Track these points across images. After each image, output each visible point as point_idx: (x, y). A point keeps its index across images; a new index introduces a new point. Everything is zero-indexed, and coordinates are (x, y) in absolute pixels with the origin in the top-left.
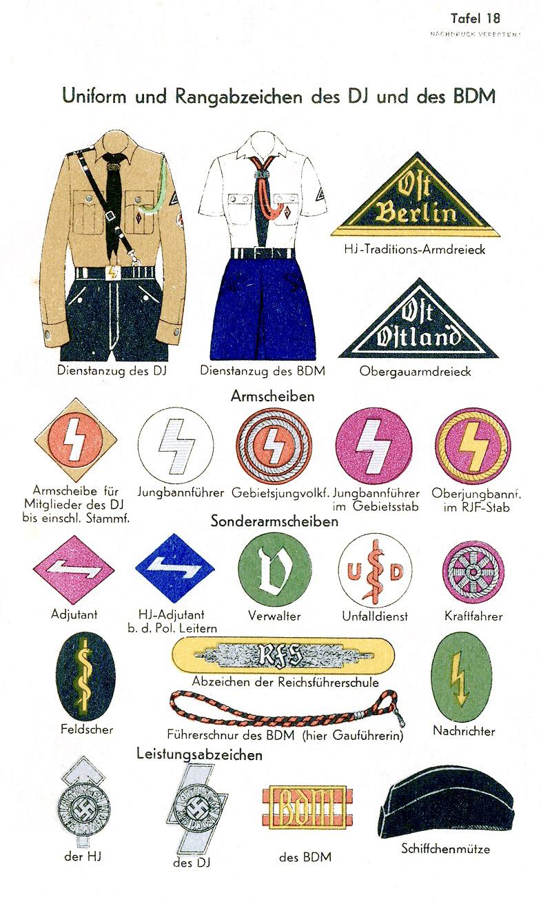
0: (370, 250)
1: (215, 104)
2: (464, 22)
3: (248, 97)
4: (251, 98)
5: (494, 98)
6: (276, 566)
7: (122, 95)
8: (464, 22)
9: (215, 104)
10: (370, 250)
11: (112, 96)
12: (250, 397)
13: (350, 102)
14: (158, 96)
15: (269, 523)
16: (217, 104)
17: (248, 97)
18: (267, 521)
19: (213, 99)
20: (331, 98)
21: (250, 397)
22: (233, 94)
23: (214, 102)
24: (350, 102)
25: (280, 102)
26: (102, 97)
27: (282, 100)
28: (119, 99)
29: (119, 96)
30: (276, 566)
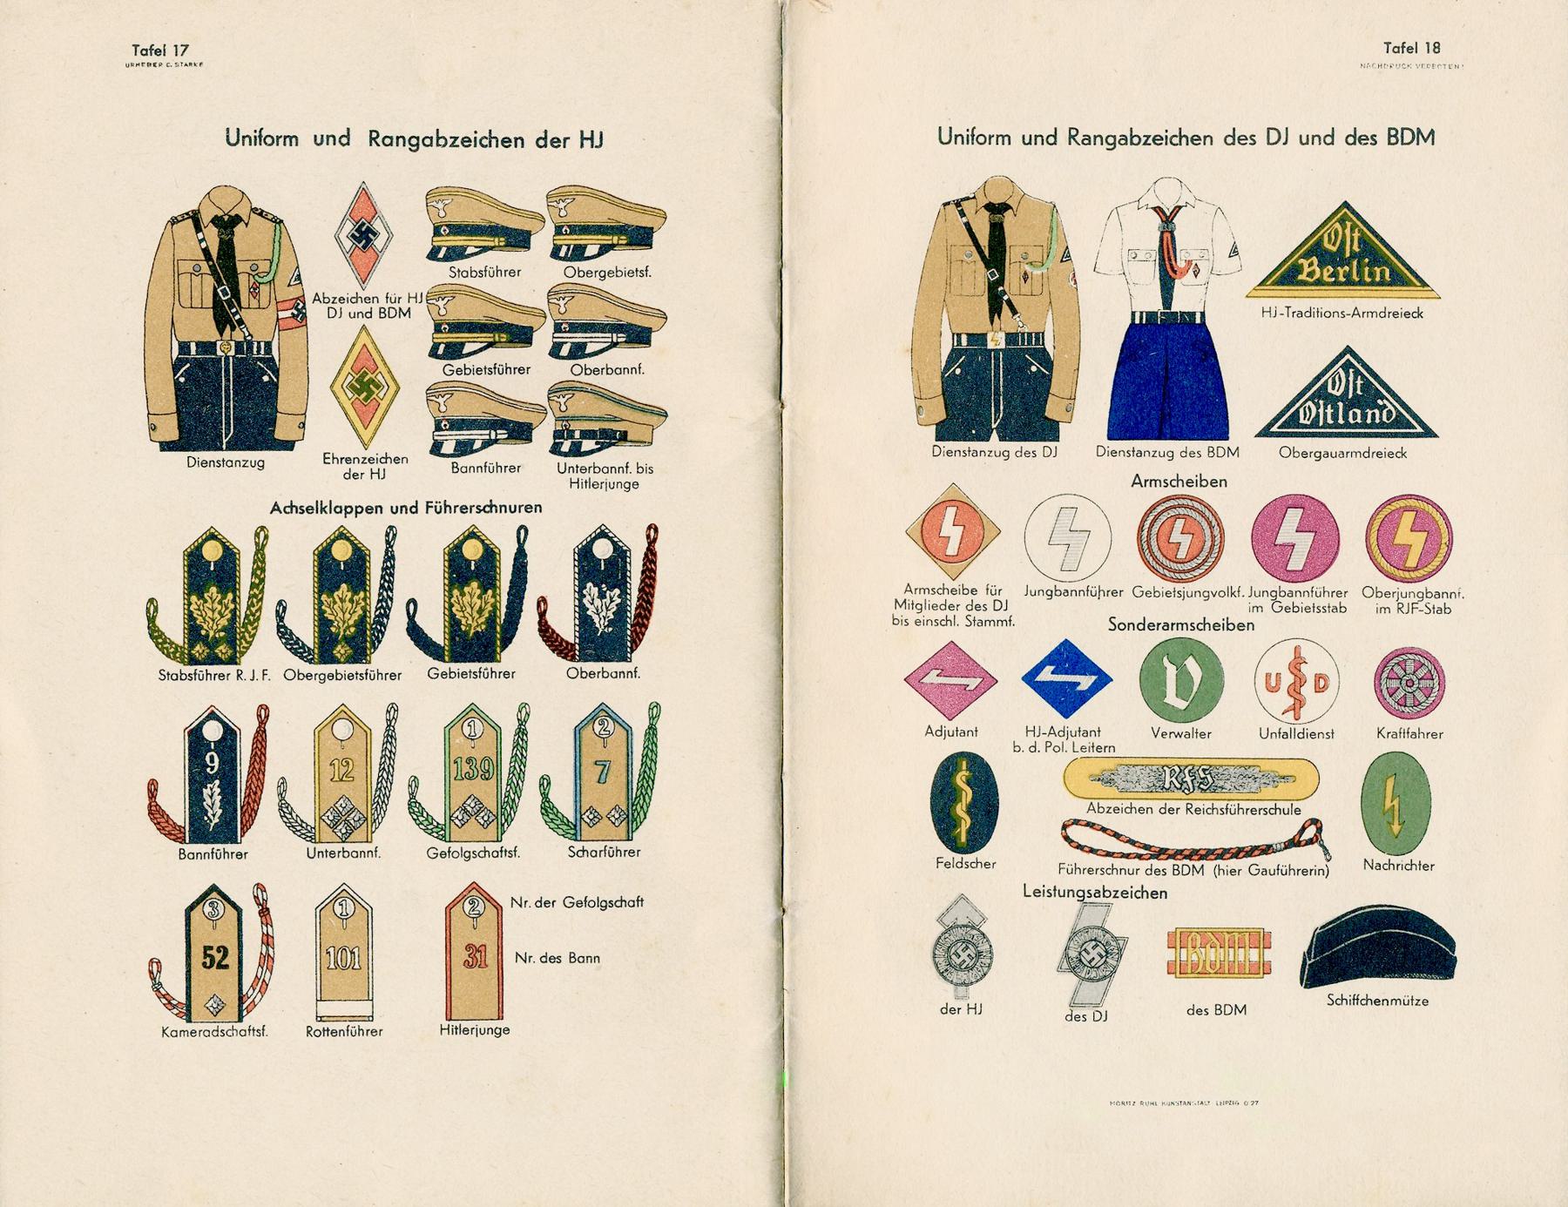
0: (1291, 314)
5: (1433, 139)
6: (1183, 677)
10: (1291, 314)
11: (995, 136)
13: (1269, 143)
24: (1269, 143)
30: (1183, 677)
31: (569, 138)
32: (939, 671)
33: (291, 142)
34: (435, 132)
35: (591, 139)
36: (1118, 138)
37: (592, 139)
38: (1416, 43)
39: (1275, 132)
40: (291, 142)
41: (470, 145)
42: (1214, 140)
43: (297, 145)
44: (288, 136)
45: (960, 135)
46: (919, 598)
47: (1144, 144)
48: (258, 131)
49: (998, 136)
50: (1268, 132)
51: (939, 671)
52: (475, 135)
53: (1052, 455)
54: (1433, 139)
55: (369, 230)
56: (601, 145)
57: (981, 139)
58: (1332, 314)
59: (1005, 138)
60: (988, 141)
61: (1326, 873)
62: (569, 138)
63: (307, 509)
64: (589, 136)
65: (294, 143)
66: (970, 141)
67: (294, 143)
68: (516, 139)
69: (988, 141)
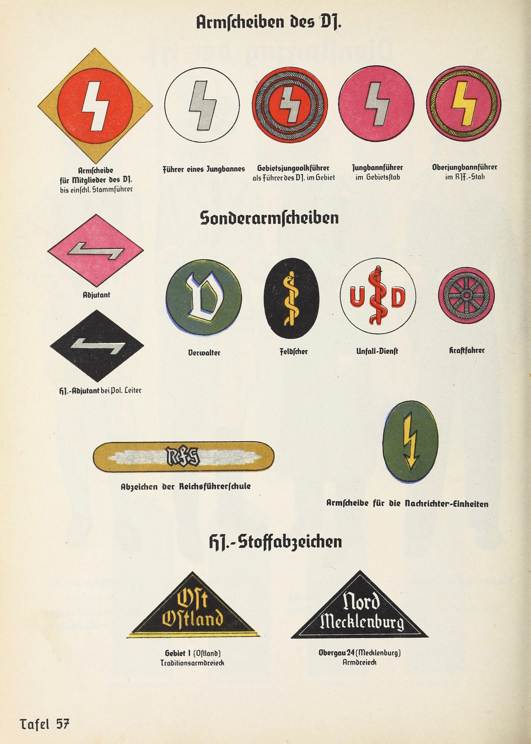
11: (358, 650)
31: (141, 389)
32: (111, 258)
33: (105, 190)
35: (191, 353)
36: (173, 655)
38: (88, 187)
39: (368, 178)
40: (105, 190)
42: (94, 193)
43: (362, 179)
45: (78, 189)
46: (85, 176)
49: (359, 650)
50: (191, 111)
51: (111, 258)
58: (229, 633)
59: (181, 170)
65: (451, 178)
67: (451, 178)
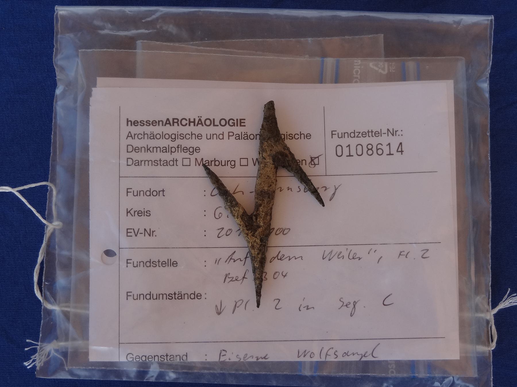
1: (234, 166)
2: (173, 165)
3: (361, 133)
4: (362, 134)
5: (253, 162)
7: (165, 294)
8: (173, 165)
9: (234, 166)
11: (356, 137)
12: (147, 162)
13: (128, 152)
14: (146, 262)
15: (143, 162)
16: (193, 153)
17: (361, 133)
18: (141, 161)
19: (173, 136)
20: (138, 123)
21: (147, 162)
22: (378, 148)
23: (192, 152)
24: (128, 152)
25: (181, 152)
26: (191, 297)
27: (133, 124)
28: (356, 63)
29: (127, 232)
34: (143, 132)
37: (194, 122)
41: (156, 125)
44: (147, 160)
47: (360, 133)
48: (153, 133)
52: (287, 133)
53: (172, 139)
54: (253, 162)
55: (261, 205)
56: (340, 301)
57: (158, 136)
60: (158, 194)
61: (181, 145)
62: (155, 231)
63: (152, 123)
64: (193, 121)
66: (135, 130)
68: (159, 121)
69: (158, 194)
